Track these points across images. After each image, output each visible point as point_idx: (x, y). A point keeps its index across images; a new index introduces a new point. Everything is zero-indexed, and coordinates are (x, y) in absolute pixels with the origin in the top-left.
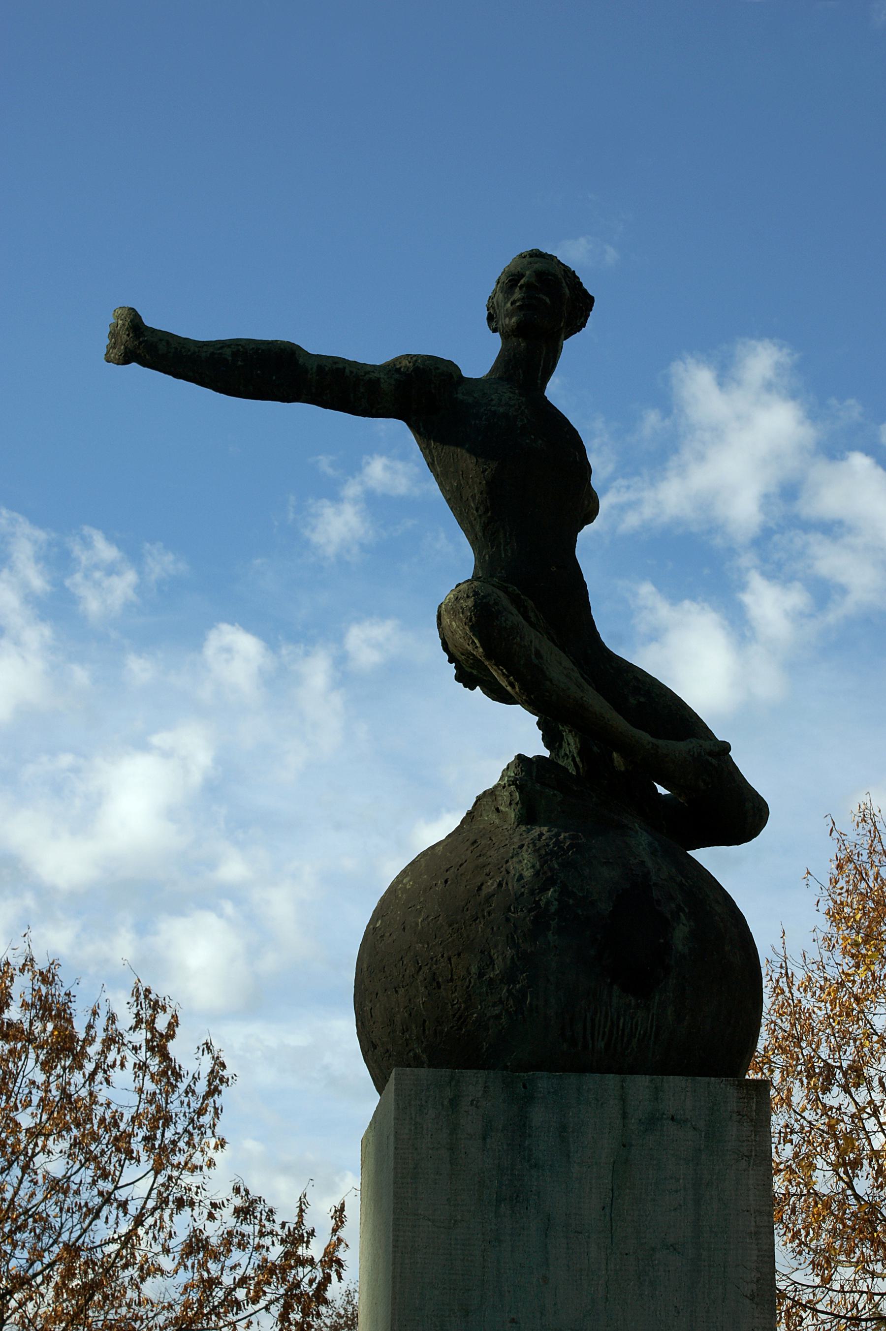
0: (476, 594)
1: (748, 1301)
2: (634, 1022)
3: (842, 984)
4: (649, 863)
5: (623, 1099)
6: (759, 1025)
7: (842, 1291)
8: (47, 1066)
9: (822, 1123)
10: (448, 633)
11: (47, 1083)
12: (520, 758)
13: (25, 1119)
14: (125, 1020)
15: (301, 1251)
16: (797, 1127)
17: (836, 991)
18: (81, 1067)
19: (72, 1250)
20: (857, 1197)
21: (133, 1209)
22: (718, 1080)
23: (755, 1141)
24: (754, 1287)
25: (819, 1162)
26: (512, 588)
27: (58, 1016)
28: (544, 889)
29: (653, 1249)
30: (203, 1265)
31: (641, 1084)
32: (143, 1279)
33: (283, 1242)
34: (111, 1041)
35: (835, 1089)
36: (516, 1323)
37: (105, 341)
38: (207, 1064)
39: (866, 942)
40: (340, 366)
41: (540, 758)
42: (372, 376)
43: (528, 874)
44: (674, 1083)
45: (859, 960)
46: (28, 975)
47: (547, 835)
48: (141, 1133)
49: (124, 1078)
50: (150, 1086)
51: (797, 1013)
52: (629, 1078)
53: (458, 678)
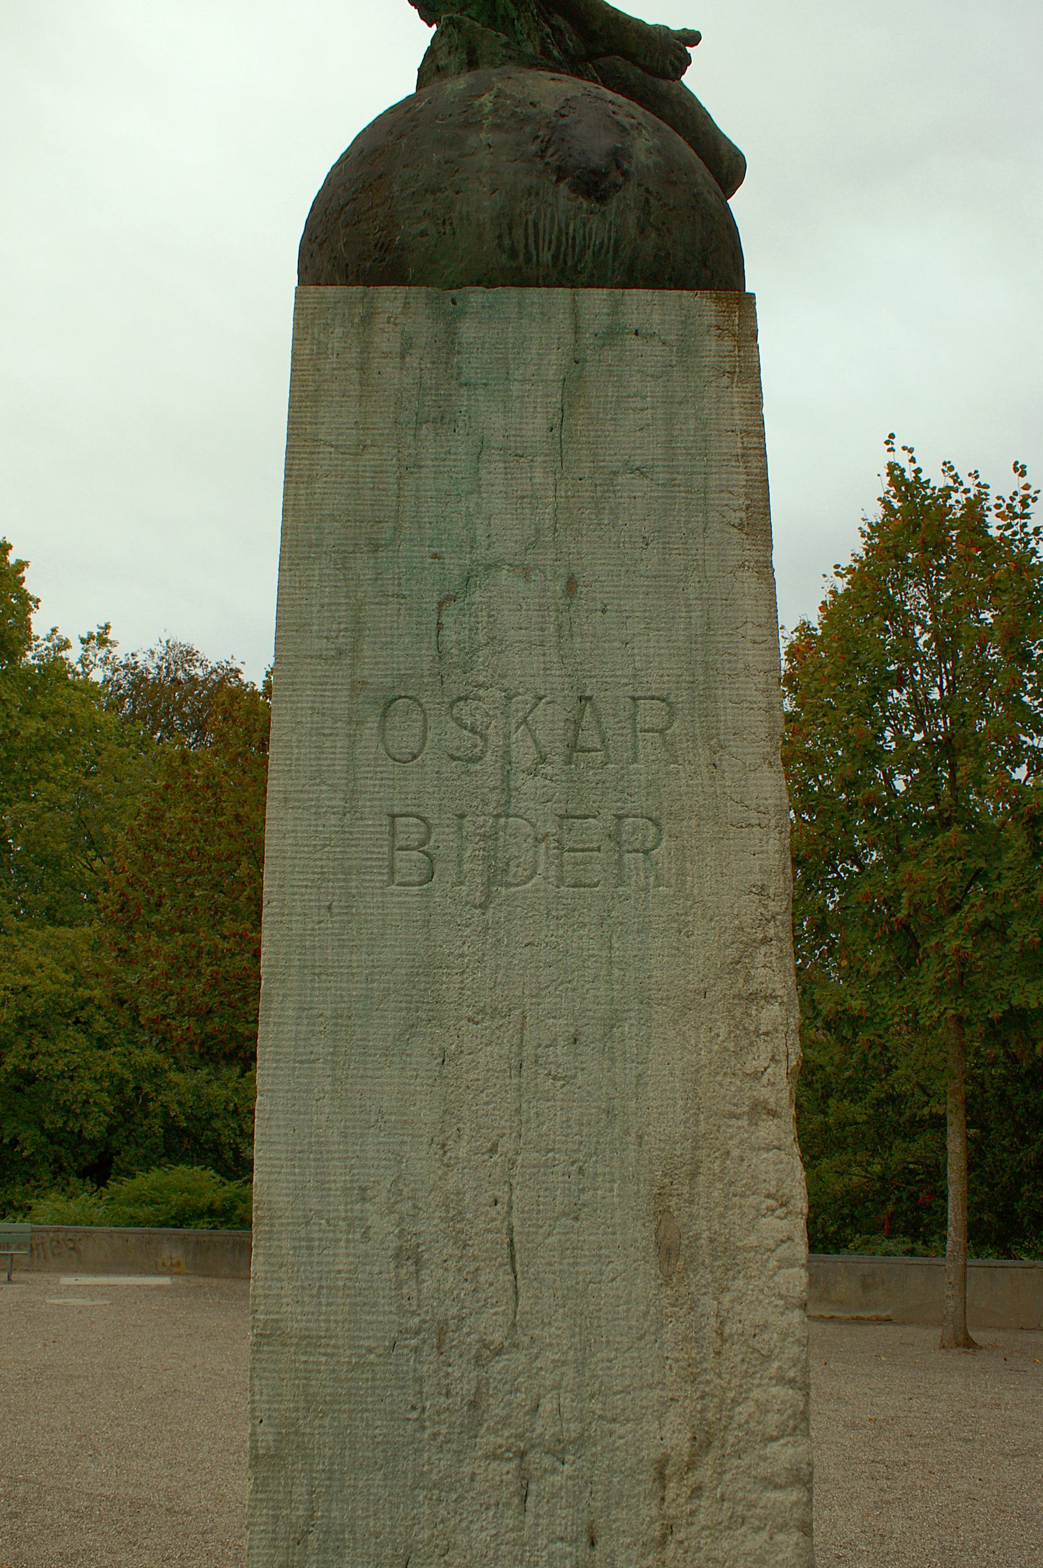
1: (736, 530)
2: (587, 230)
12: (10, 547)
22: (692, 293)
23: (739, 356)
24: (743, 515)
29: (615, 473)
36: (439, 558)
44: (637, 298)
52: (582, 291)
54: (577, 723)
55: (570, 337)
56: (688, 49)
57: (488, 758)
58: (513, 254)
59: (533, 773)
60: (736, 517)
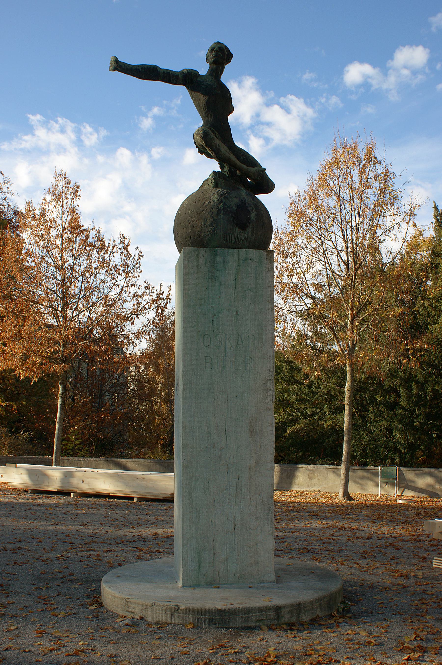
0: (203, 130)
3: (291, 233)
4: (245, 198)
5: (239, 255)
6: (270, 242)
7: (289, 305)
8: (99, 253)
9: (285, 265)
10: (196, 140)
11: (99, 257)
12: (214, 171)
13: (94, 265)
14: (117, 242)
15: (161, 296)
16: (279, 266)
17: (289, 234)
18: (107, 253)
19: (107, 296)
20: (293, 283)
21: (120, 287)
25: (284, 275)
26: (212, 129)
27: (101, 240)
28: (220, 204)
30: (138, 300)
31: (243, 251)
32: (123, 303)
33: (156, 294)
34: (114, 247)
35: (289, 258)
37: (109, 65)
38: (138, 252)
39: (297, 222)
40: (169, 71)
41: (219, 172)
42: (177, 74)
43: (216, 200)
44: (251, 251)
45: (295, 227)
46: (94, 231)
47: (220, 191)
48: (122, 269)
49: (117, 256)
50: (124, 258)
51: (279, 240)
53: (199, 152)
54: (238, 340)
55: (238, 260)
56: (260, 197)
57: (222, 346)
58: (227, 241)
59: (230, 349)
60: (268, 299)
